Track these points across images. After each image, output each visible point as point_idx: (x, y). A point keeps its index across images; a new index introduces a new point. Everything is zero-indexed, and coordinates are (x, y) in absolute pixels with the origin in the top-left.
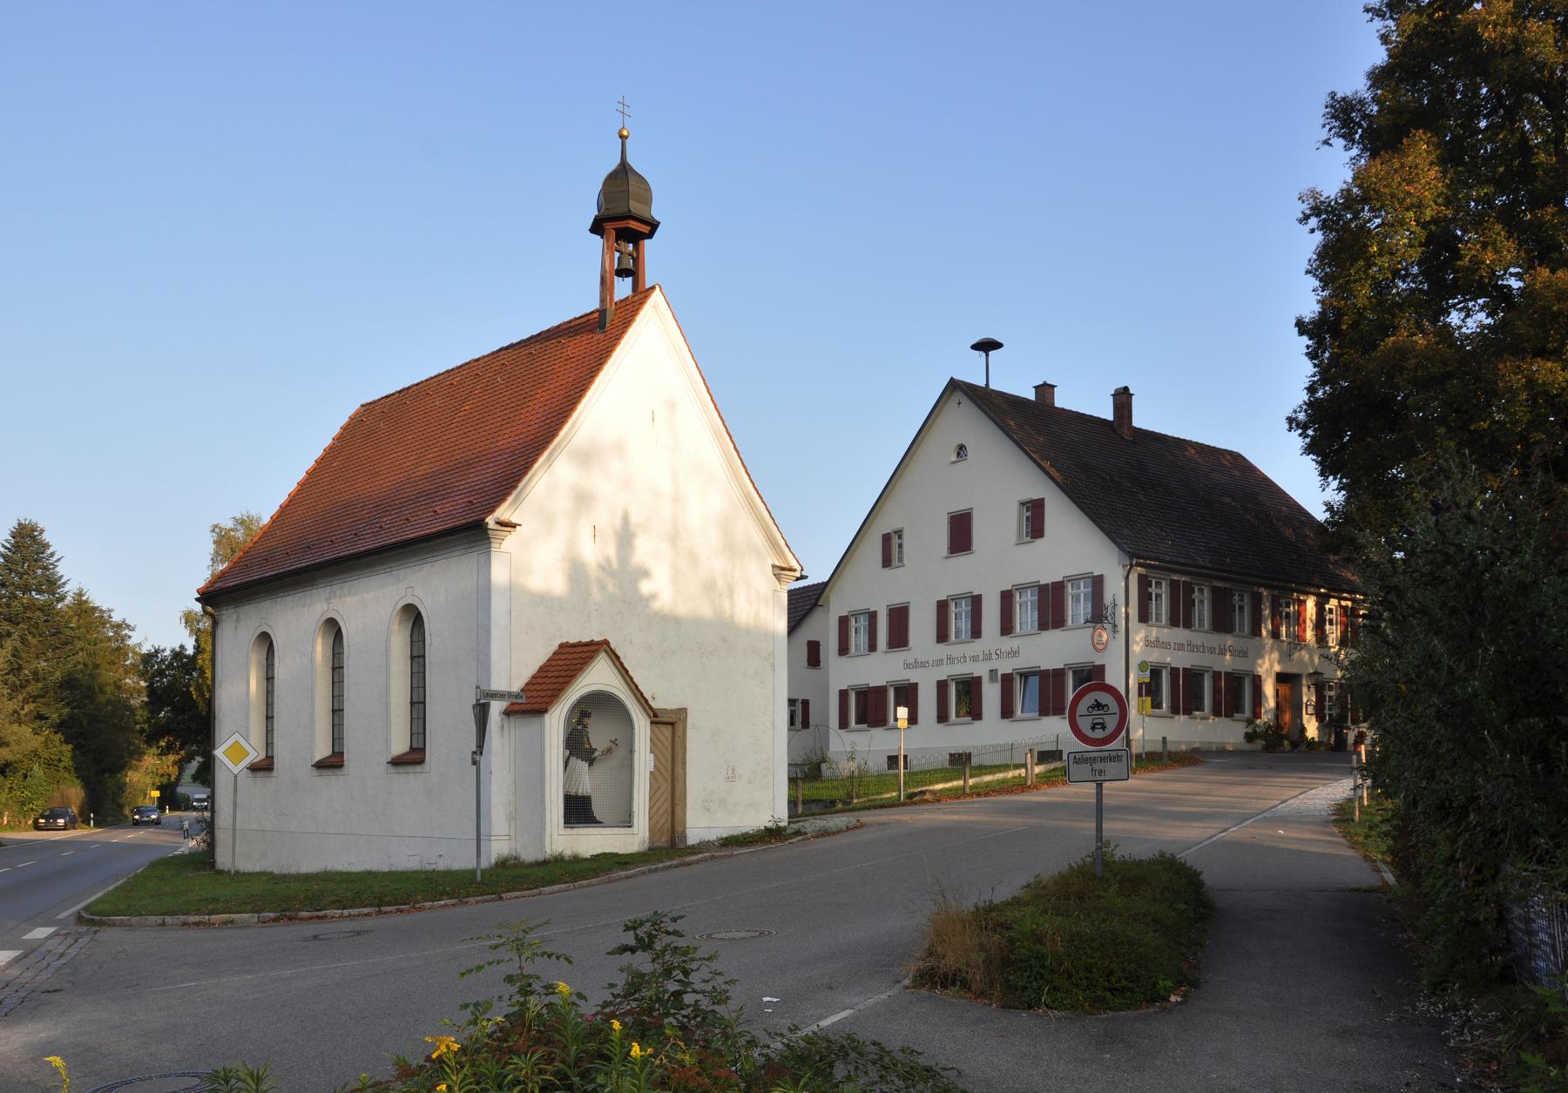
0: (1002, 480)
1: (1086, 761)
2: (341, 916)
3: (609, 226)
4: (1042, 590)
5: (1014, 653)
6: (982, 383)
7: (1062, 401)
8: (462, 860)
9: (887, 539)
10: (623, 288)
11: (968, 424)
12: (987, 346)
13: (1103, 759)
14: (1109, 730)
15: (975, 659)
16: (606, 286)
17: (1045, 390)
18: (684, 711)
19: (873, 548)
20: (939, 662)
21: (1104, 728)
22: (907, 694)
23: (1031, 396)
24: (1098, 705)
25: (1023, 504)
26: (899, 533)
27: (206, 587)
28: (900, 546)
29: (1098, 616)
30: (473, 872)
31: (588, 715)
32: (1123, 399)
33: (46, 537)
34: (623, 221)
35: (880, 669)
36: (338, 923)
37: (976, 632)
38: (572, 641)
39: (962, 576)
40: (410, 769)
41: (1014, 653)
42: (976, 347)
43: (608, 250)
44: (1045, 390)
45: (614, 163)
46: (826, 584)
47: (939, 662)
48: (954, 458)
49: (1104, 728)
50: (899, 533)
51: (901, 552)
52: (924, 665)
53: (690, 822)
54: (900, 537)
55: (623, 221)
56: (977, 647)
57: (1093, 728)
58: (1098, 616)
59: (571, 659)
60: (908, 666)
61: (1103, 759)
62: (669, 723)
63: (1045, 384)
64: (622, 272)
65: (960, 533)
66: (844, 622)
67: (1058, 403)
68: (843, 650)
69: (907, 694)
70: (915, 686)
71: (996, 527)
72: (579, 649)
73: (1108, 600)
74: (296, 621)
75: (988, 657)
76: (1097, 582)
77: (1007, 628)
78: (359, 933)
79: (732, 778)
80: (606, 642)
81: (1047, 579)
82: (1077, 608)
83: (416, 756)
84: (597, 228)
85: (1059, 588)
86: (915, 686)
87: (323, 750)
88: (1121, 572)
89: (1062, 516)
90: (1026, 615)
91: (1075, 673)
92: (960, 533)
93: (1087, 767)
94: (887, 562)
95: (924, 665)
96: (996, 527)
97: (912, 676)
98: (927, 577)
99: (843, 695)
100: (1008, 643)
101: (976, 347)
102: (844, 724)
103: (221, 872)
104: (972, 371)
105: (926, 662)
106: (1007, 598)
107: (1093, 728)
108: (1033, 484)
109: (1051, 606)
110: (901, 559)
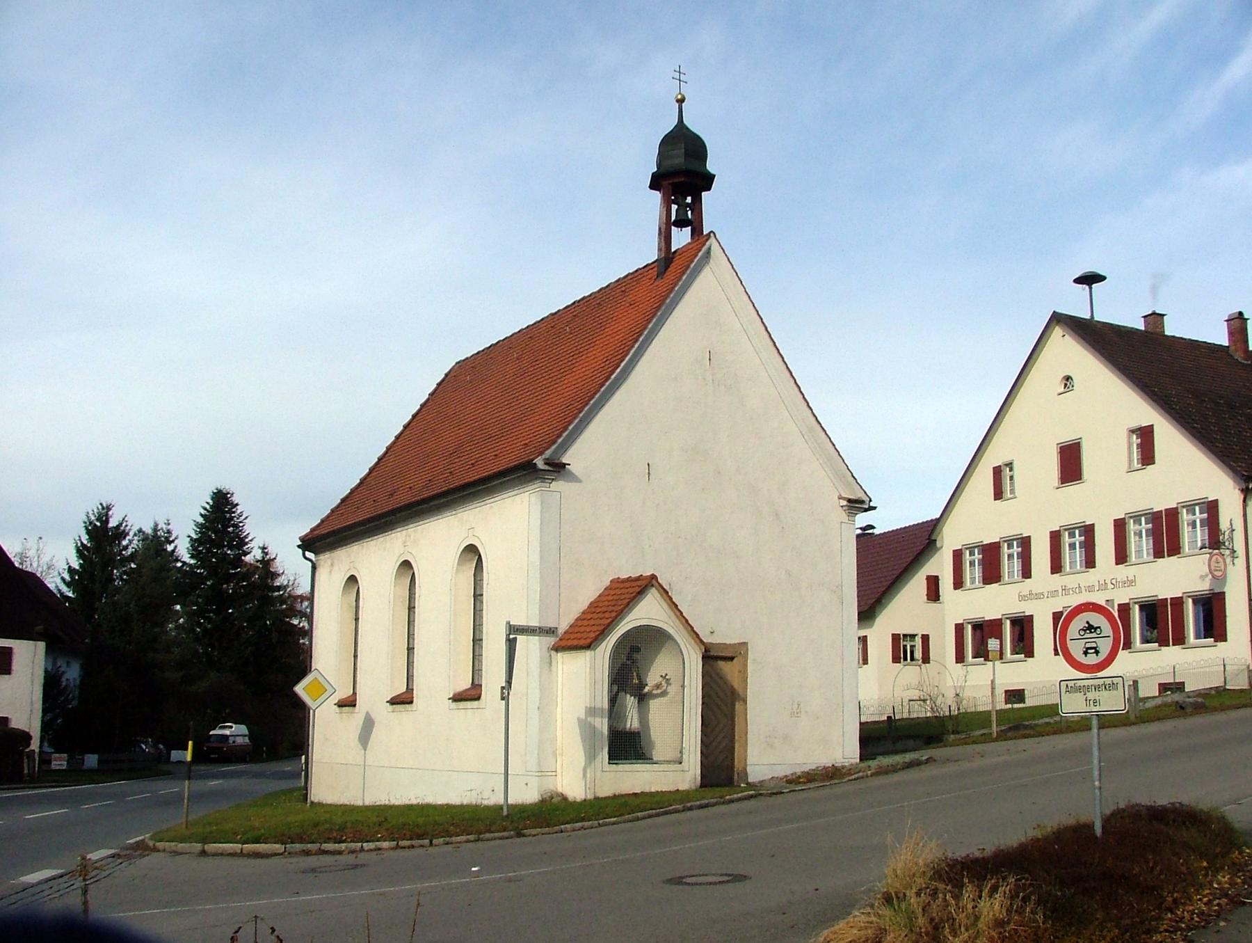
0: (1111, 407)
1: (1079, 689)
2: (362, 849)
3: (665, 183)
4: (1155, 517)
5: (1130, 583)
6: (1088, 317)
7: (1172, 328)
8: (491, 796)
9: (997, 472)
10: (681, 238)
11: (1068, 352)
12: (1089, 279)
13: (1097, 688)
14: (1104, 653)
15: (1090, 589)
16: (666, 237)
17: (1155, 319)
18: (745, 644)
19: (983, 480)
20: (1054, 594)
21: (1097, 652)
22: (1023, 627)
23: (1141, 326)
24: (1090, 628)
25: (1132, 431)
26: (1010, 465)
27: (306, 535)
28: (1011, 478)
29: (1215, 541)
30: (501, 807)
31: (638, 650)
32: (1238, 324)
33: (235, 499)
34: (682, 173)
35: (994, 602)
36: (440, 849)
37: (1090, 562)
38: (624, 576)
39: (1075, 505)
40: (469, 704)
41: (1130, 583)
42: (1079, 281)
43: (667, 204)
44: (1155, 319)
45: (670, 124)
46: (938, 521)
47: (1054, 594)
48: (1062, 390)
49: (1097, 652)
50: (1010, 465)
51: (1012, 484)
52: (1039, 596)
53: (750, 760)
54: (1011, 470)
55: (682, 173)
56: (1092, 576)
57: (1086, 653)
58: (1215, 541)
59: (631, 590)
60: (1022, 598)
61: (1097, 688)
62: (713, 657)
63: (1154, 313)
64: (681, 223)
65: (1070, 463)
66: (958, 555)
67: (1169, 331)
68: (958, 583)
69: (1023, 627)
70: (1030, 619)
71: (1106, 456)
72: (627, 585)
73: (1224, 525)
74: (374, 559)
75: (1103, 587)
76: (1212, 508)
77: (1121, 557)
78: (355, 867)
79: (796, 713)
80: (654, 577)
81: (1160, 506)
82: (1192, 534)
83: (473, 693)
84: (655, 185)
85: (1173, 515)
86: (1030, 619)
87: (465, 684)
88: (1237, 496)
89: (1169, 437)
90: (1140, 544)
91: (1195, 602)
92: (1070, 463)
93: (1080, 697)
94: (998, 494)
95: (1039, 596)
96: (1106, 456)
97: (1027, 608)
98: (1039, 508)
99: (959, 629)
100: (1123, 571)
101: (1079, 281)
102: (960, 658)
103: (759, 791)
104: (1076, 303)
105: (1039, 595)
106: (1120, 527)
107: (1086, 653)
108: (1144, 412)
109: (1165, 533)
110: (1012, 491)
